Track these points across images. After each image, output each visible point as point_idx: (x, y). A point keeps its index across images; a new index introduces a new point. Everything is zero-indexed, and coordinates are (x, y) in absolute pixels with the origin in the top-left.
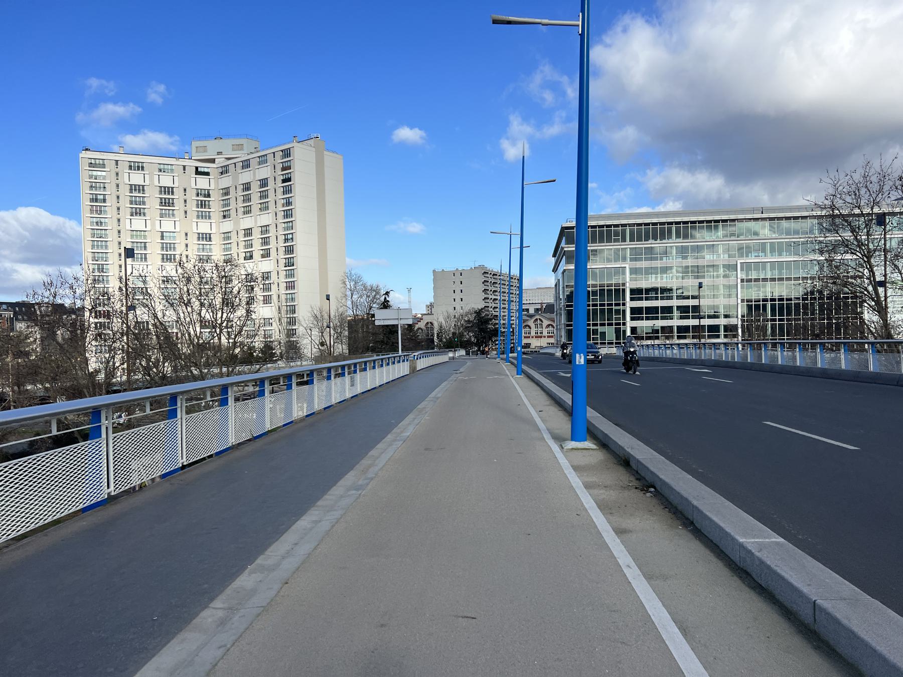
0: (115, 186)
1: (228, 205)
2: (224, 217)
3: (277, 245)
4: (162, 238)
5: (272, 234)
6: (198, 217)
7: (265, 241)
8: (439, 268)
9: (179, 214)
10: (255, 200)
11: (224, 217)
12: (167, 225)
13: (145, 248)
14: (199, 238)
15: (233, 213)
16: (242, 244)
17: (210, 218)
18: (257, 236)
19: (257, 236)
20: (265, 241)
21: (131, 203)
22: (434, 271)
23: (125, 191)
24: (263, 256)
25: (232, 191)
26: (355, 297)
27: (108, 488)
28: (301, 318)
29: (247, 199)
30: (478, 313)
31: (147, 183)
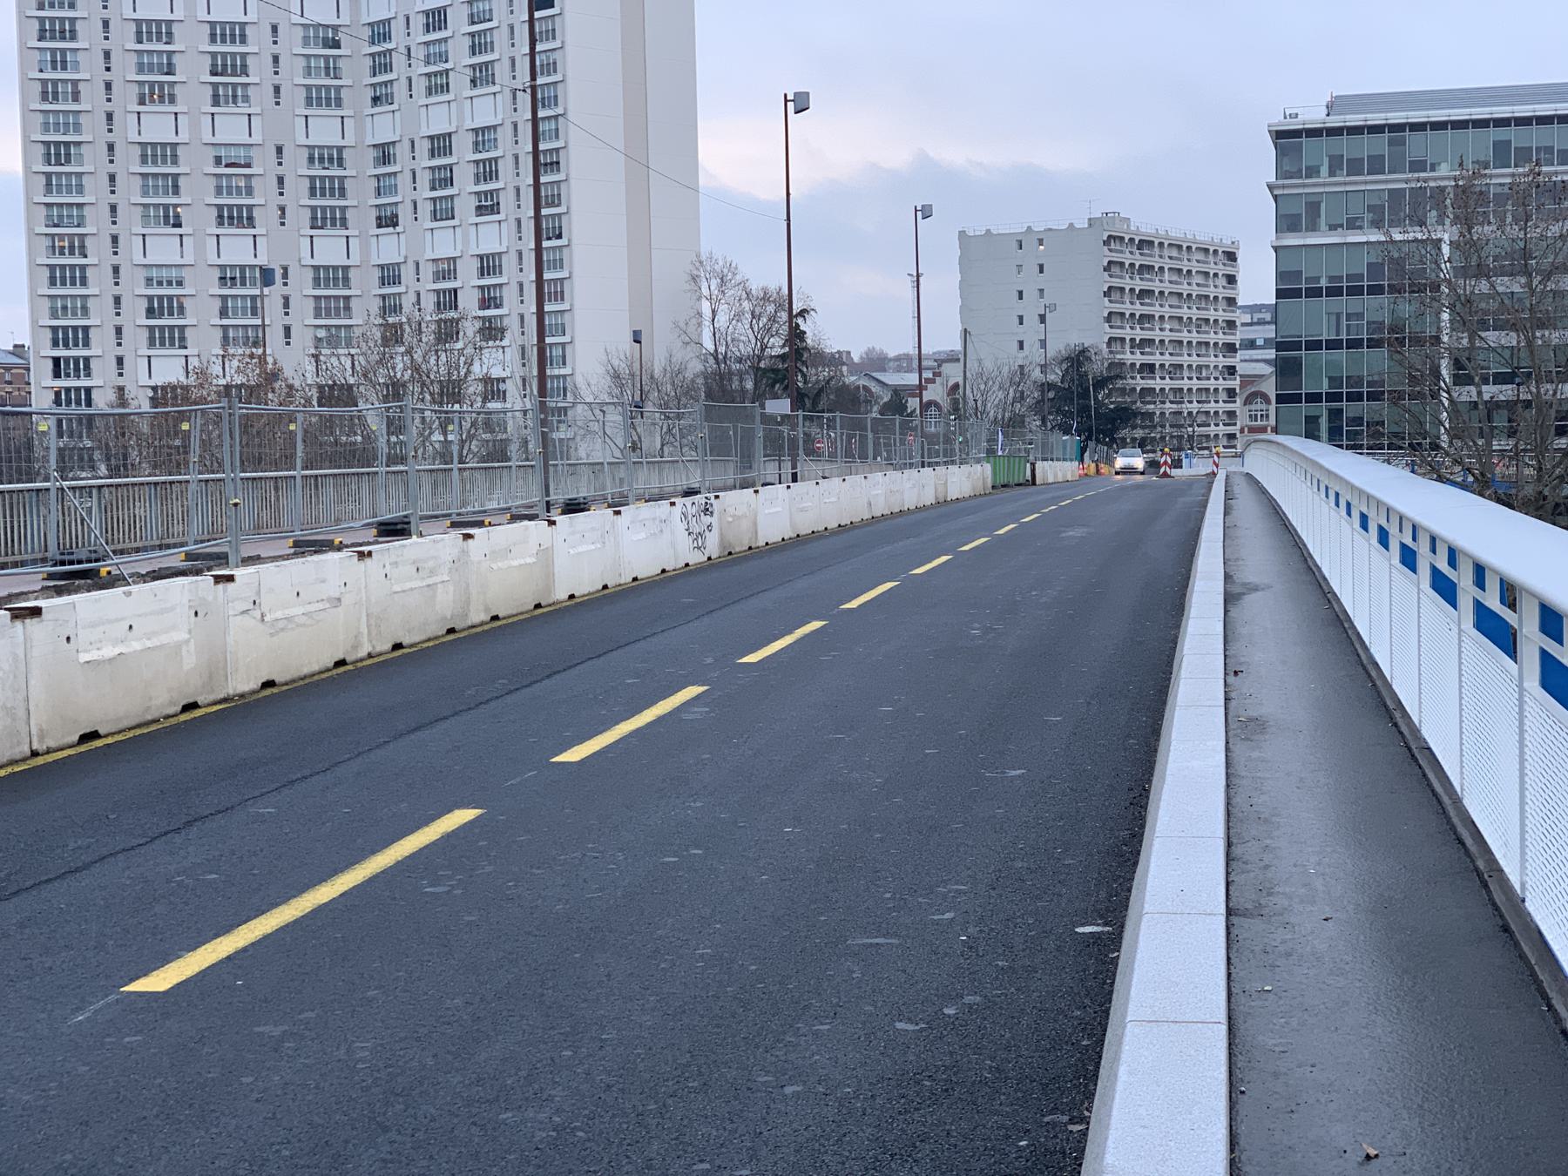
0: (111, 301)
1: (388, 68)
2: (376, 100)
3: (514, 179)
4: (223, 313)
5: (503, 149)
6: (309, 102)
7: (487, 171)
8: (976, 228)
9: (261, 98)
10: (465, 185)
11: (376, 100)
12: (231, 128)
13: (176, 190)
14: (311, 159)
15: (400, 90)
16: (424, 179)
17: (344, 225)
18: (463, 154)
19: (463, 154)
20: (487, 171)
21: (141, 69)
22: (962, 234)
23: (129, 163)
24: (480, 210)
25: (402, 152)
26: (722, 320)
27: (114, 552)
28: (579, 380)
29: (443, 178)
30: (1077, 359)
31: (183, 137)
